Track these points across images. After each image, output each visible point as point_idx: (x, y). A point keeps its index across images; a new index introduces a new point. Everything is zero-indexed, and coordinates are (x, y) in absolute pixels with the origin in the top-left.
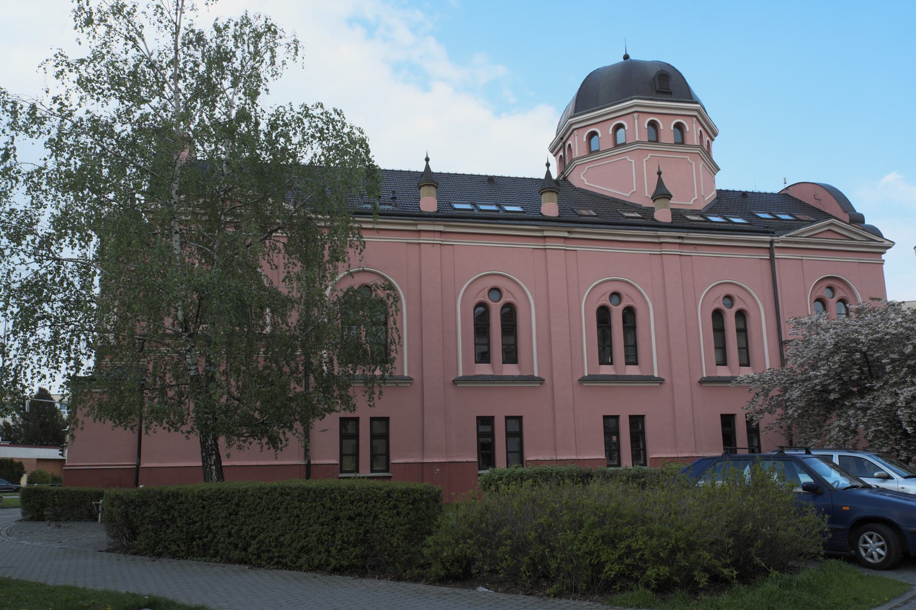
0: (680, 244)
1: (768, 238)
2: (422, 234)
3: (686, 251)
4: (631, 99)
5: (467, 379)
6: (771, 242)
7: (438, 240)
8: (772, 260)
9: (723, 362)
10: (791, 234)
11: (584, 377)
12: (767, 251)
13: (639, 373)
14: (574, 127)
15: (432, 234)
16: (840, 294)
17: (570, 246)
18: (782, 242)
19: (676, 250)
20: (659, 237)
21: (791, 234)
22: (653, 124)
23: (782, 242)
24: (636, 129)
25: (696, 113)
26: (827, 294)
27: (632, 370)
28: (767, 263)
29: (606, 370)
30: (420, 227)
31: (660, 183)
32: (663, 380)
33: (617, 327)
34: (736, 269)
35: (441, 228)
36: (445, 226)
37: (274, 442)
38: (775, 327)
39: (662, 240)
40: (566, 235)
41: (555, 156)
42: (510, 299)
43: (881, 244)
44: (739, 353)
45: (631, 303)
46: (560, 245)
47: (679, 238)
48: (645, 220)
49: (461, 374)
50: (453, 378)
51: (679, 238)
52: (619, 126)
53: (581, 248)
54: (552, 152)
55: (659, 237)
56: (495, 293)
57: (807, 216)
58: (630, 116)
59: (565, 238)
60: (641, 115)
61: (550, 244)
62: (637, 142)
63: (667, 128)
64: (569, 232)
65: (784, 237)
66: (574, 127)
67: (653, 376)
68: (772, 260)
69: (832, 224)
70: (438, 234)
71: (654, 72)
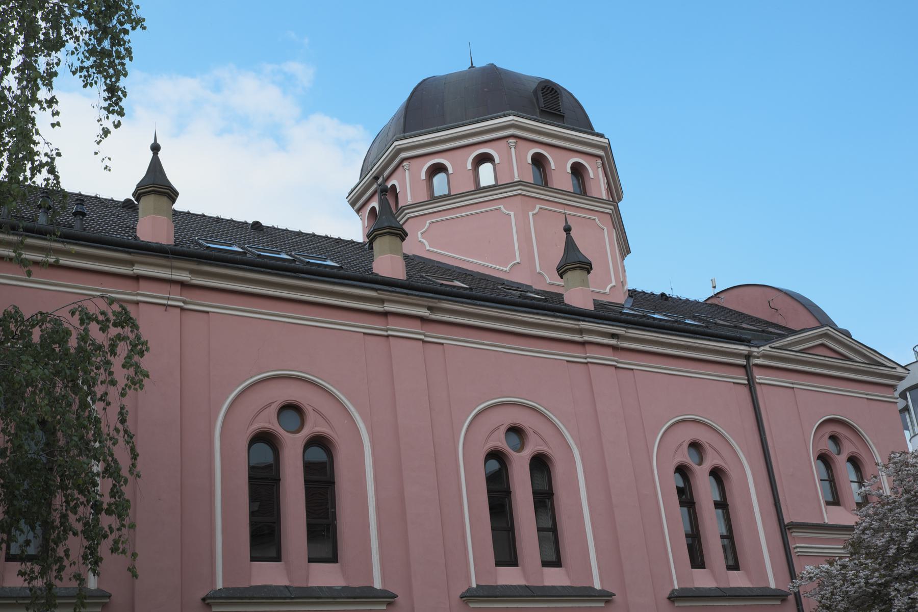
0: (615, 348)
1: (743, 349)
2: (142, 283)
3: (625, 361)
4: (505, 116)
5: (233, 596)
6: (748, 357)
7: (176, 297)
8: (751, 385)
9: (507, 554)
10: (777, 344)
11: (470, 589)
12: (743, 371)
13: (566, 582)
14: (404, 155)
15: (166, 287)
16: (849, 448)
17: (433, 334)
18: (765, 356)
19: (608, 357)
20: (581, 331)
21: (777, 344)
22: (539, 161)
23: (765, 356)
24: (515, 162)
25: (602, 153)
26: (830, 447)
27: (554, 577)
28: (745, 391)
29: (509, 577)
30: (139, 270)
31: (570, 245)
32: (612, 595)
33: (518, 492)
34: (696, 394)
35: (185, 277)
36: (192, 272)
37: (123, 327)
38: (770, 500)
39: (587, 338)
40: (424, 312)
41: (358, 211)
42: (322, 428)
43: (892, 372)
44: (541, 540)
45: (542, 448)
46: (414, 330)
47: (613, 336)
48: (551, 305)
49: (220, 585)
50: (203, 594)
51: (613, 336)
52: (485, 158)
53: (452, 340)
54: (353, 204)
55: (581, 331)
56: (291, 414)
57: (740, 329)
58: (504, 142)
59: (423, 319)
60: (521, 142)
61: (396, 327)
62: (519, 183)
63: (560, 167)
64: (430, 308)
65: (767, 348)
66: (404, 155)
67: (593, 589)
68: (751, 385)
69: (826, 335)
70: (178, 288)
71: (534, 86)
